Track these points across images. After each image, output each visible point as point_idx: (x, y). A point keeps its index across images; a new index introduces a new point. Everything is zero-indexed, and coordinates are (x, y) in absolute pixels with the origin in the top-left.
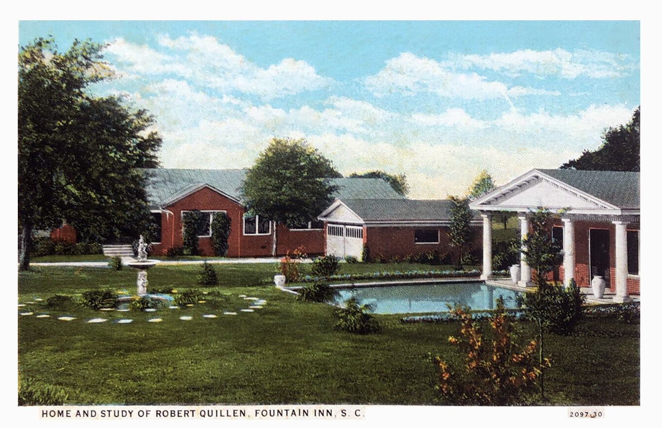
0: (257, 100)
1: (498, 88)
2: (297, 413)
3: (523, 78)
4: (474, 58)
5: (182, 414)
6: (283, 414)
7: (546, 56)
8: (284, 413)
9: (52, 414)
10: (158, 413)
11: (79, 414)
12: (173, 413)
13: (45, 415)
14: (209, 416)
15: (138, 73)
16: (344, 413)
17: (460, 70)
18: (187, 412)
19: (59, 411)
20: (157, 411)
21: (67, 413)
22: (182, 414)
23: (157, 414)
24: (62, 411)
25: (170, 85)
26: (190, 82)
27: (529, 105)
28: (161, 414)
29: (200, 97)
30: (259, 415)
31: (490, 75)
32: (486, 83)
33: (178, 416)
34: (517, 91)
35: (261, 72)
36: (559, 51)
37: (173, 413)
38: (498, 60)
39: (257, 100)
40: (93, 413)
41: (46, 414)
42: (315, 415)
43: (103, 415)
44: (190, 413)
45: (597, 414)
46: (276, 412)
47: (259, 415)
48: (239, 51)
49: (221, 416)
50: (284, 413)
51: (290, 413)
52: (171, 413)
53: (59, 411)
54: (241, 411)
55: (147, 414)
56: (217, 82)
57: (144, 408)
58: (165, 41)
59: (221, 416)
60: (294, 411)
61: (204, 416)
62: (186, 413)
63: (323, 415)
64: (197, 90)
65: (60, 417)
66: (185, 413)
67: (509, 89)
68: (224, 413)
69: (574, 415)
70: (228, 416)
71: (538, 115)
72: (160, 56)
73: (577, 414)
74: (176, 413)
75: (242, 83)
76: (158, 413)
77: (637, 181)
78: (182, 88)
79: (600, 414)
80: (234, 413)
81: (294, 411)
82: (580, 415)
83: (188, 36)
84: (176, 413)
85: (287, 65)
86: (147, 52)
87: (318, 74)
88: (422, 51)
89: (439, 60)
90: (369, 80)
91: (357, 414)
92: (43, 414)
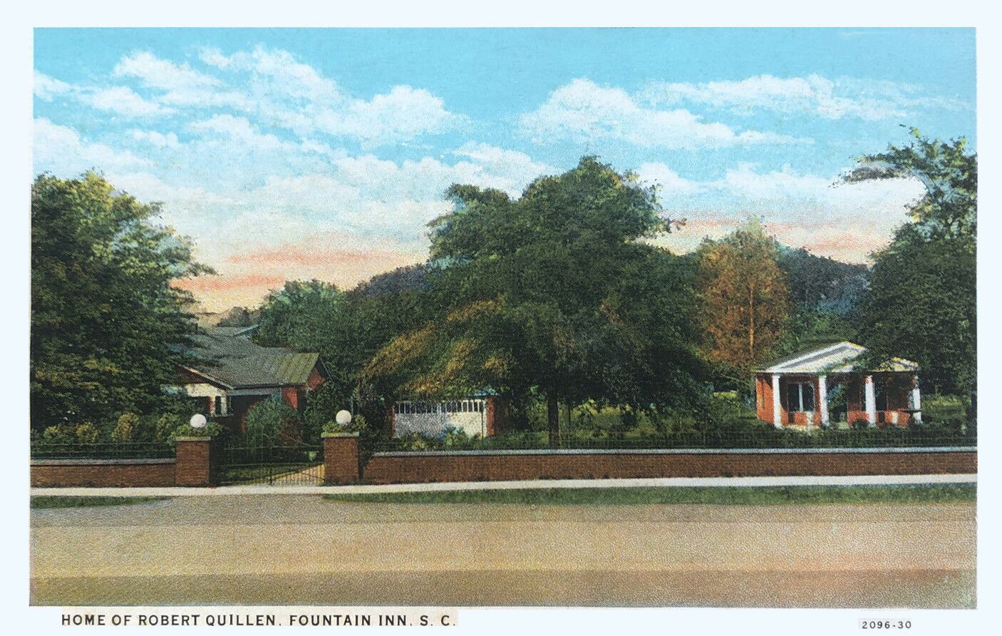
0: (352, 146)
1: (722, 133)
2: (353, 620)
3: (765, 118)
4: (680, 89)
5: (179, 620)
6: (332, 623)
7: (795, 87)
8: (334, 620)
9: (76, 620)
10: (142, 620)
11: (350, 622)
12: (164, 620)
13: (66, 622)
14: (313, 624)
15: (172, 106)
16: (424, 621)
17: (662, 106)
18: (185, 618)
19: (87, 616)
20: (140, 616)
21: (100, 620)
22: (179, 620)
23: (140, 620)
24: (93, 616)
25: (220, 123)
26: (253, 120)
27: (767, 160)
28: (147, 621)
29: (271, 141)
30: (296, 623)
31: (705, 114)
32: (699, 125)
33: (173, 624)
34: (752, 137)
35: (360, 105)
36: (815, 79)
37: (164, 620)
38: (720, 91)
39: (352, 146)
40: (117, 622)
41: (68, 620)
42: (381, 624)
43: (424, 623)
44: (191, 621)
45: (904, 625)
46: (321, 619)
47: (296, 623)
48: (326, 74)
49: (238, 624)
50: (334, 620)
51: (342, 620)
52: (163, 620)
53: (87, 616)
54: (268, 617)
55: (126, 620)
56: (296, 120)
57: (122, 611)
58: (214, 57)
59: (238, 624)
60: (348, 617)
61: (212, 624)
62: (185, 620)
63: (392, 623)
64: (264, 132)
65: (89, 626)
66: (183, 620)
67: (737, 134)
68: (243, 620)
69: (868, 626)
70: (248, 624)
71: (782, 174)
72: (206, 79)
73: (873, 625)
74: (170, 620)
75: (331, 122)
76: (142, 620)
77: (36, 561)
78: (240, 128)
79: (908, 625)
80: (258, 620)
81: (348, 617)
82: (877, 625)
83: (249, 50)
84: (170, 620)
85: (402, 95)
86: (188, 75)
87: (446, 109)
88: (601, 77)
89: (631, 92)
90: (528, 119)
91: (444, 622)
92: (64, 620)
